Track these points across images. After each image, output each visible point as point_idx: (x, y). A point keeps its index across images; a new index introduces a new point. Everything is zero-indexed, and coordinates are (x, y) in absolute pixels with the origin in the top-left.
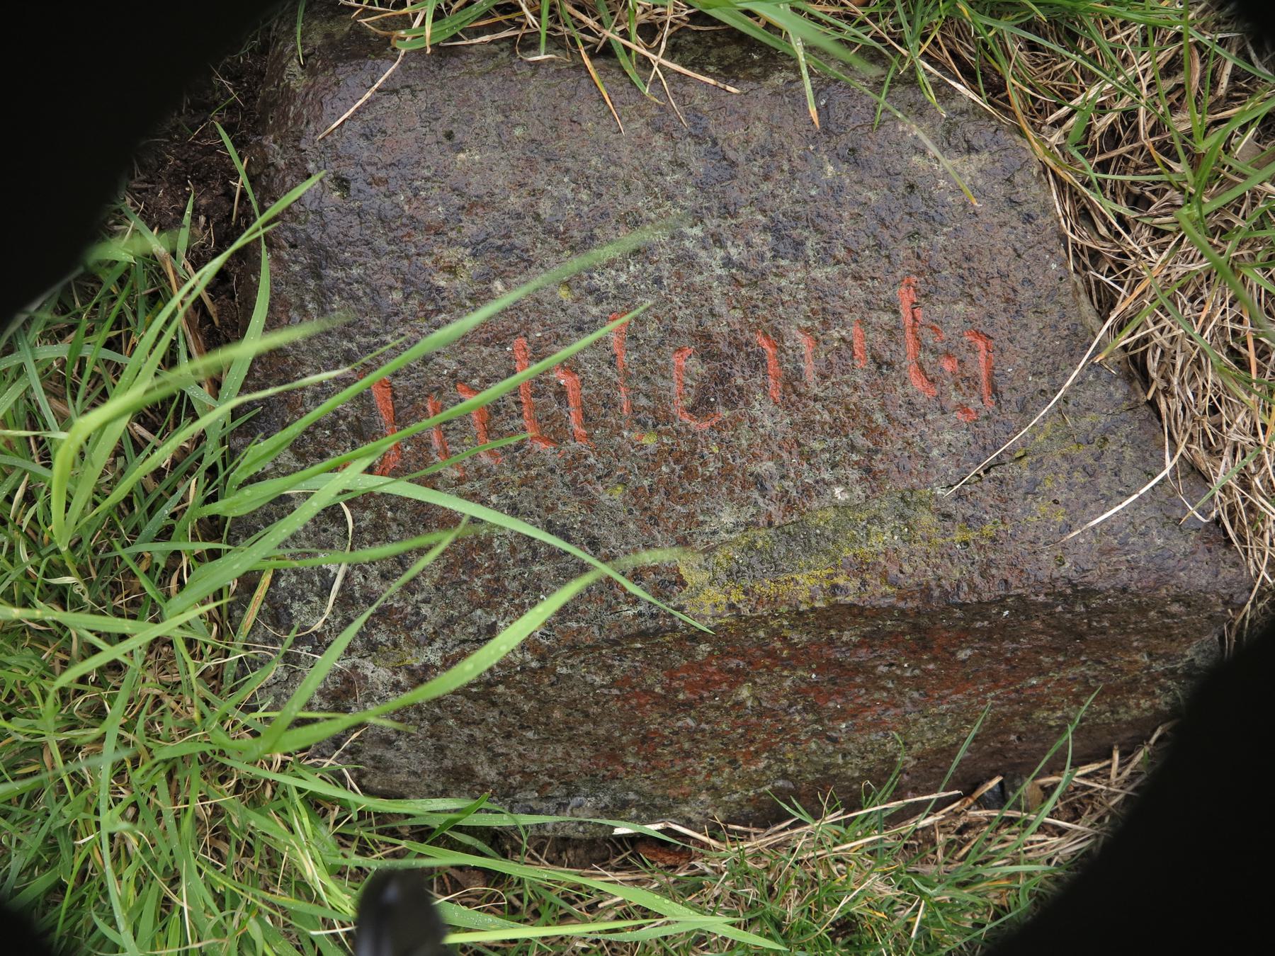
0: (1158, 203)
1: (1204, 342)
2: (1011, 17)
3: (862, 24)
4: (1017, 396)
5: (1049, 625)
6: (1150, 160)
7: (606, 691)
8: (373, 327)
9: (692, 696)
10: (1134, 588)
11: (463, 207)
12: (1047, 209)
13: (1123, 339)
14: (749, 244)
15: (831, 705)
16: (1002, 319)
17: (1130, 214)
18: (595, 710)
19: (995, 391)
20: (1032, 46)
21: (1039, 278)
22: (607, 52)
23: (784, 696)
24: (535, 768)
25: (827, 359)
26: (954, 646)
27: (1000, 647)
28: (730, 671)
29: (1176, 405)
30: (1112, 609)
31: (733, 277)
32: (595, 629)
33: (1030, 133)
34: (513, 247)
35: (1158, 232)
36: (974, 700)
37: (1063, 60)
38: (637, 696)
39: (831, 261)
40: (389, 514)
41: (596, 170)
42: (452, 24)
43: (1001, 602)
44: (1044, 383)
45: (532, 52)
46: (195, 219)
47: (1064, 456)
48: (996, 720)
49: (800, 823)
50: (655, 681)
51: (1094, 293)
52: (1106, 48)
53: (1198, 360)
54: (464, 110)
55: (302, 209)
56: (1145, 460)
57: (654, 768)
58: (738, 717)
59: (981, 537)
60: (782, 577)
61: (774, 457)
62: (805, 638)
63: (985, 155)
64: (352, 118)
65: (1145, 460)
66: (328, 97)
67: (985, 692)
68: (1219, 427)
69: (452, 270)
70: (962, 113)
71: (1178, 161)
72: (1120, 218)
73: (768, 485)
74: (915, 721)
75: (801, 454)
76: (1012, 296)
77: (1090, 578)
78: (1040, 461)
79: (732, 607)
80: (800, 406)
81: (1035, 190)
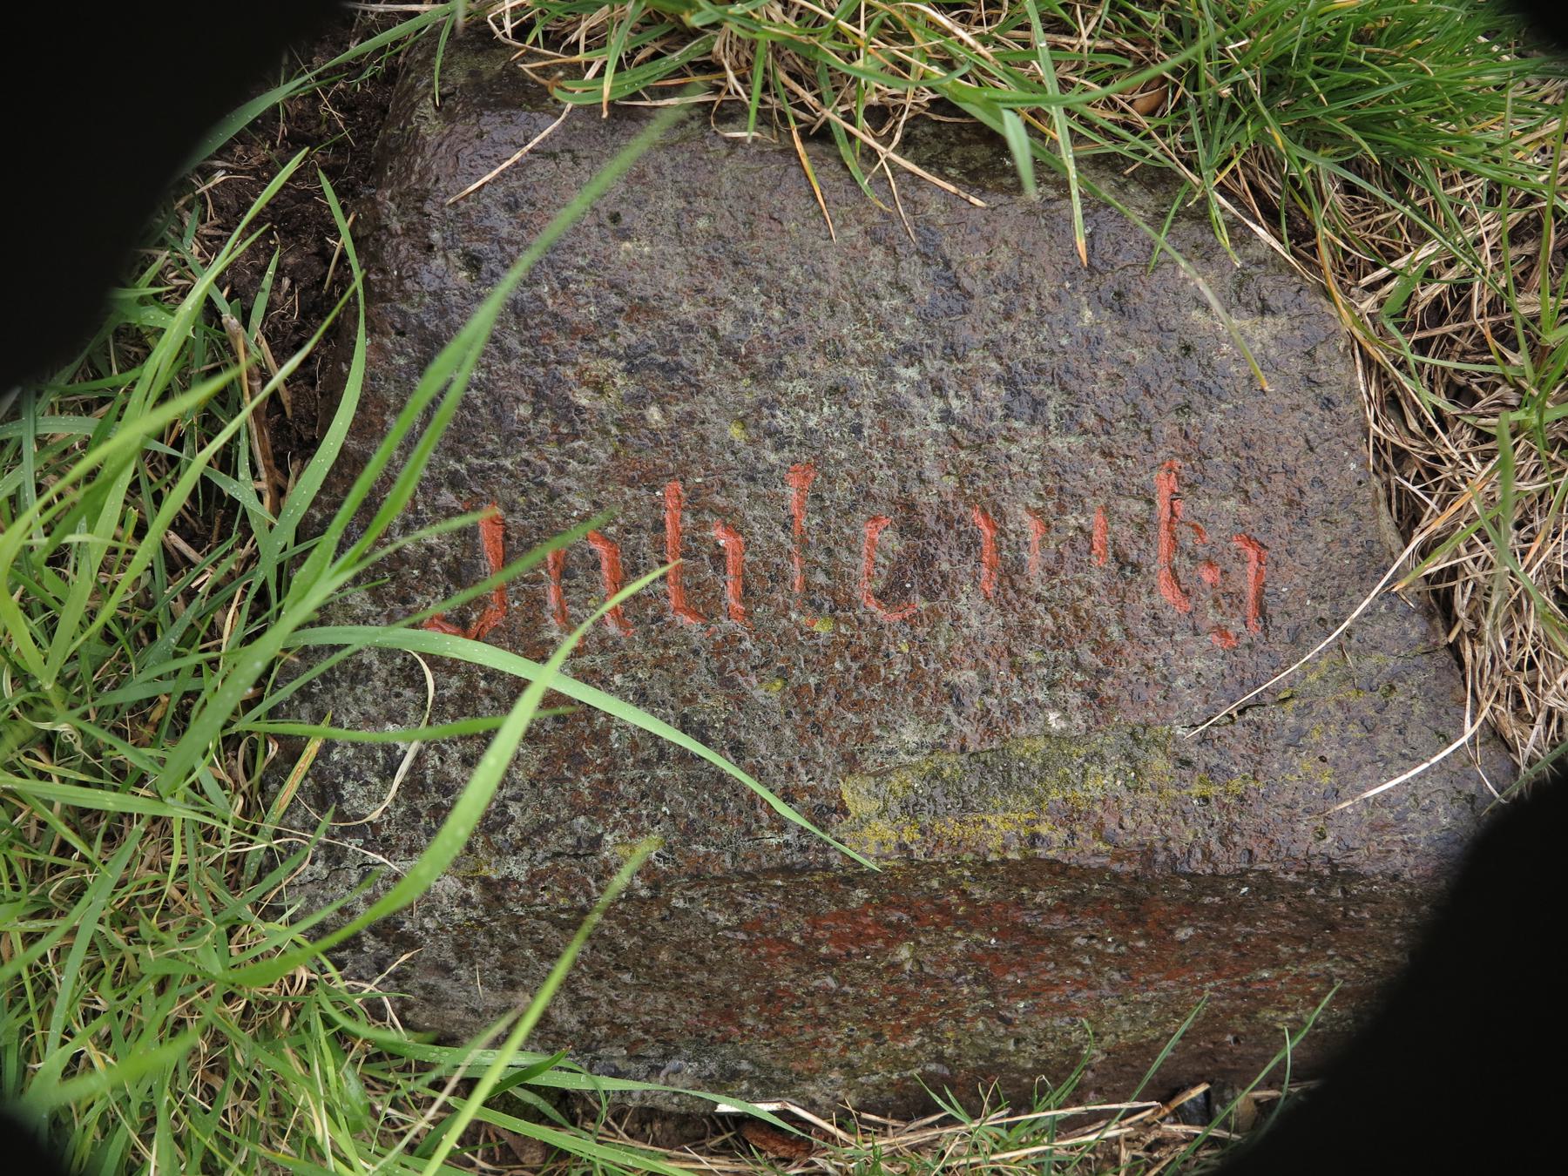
0: (1486, 399)
1: (1529, 579)
2: (1331, 151)
3: (1148, 137)
4: (1291, 623)
5: (1295, 910)
6: (1481, 343)
7: (730, 935)
8: (490, 447)
9: (838, 951)
10: (1407, 876)
11: (622, 310)
12: (1351, 393)
13: (1431, 567)
14: (976, 397)
15: (1010, 978)
16: (1282, 525)
17: (1450, 410)
18: (713, 956)
19: (1262, 610)
20: (1349, 188)
21: (1333, 481)
22: (822, 136)
23: (953, 963)
24: (627, 1019)
25: (1058, 551)
26: (1173, 922)
27: (1231, 930)
28: (890, 925)
29: (1484, 654)
30: (1375, 899)
31: (950, 433)
32: (727, 858)
33: (1338, 296)
34: (679, 366)
35: (1483, 436)
36: (1188, 990)
37: (1387, 210)
38: (768, 944)
39: (1077, 430)
40: (483, 684)
41: (795, 282)
42: (635, 79)
43: (1240, 877)
44: (1324, 610)
45: (730, 125)
46: (277, 281)
47: (1339, 703)
48: (1211, 1016)
49: (949, 1121)
50: (794, 928)
51: (1394, 500)
52: (1444, 202)
53: (1518, 603)
54: (637, 188)
55: (417, 287)
56: (1438, 717)
57: (777, 1034)
58: (891, 982)
59: (1226, 794)
60: (970, 817)
61: (977, 665)
62: (988, 894)
63: (1283, 320)
64: (495, 181)
65: (1438, 717)
66: (467, 152)
67: (1202, 981)
68: (1533, 686)
69: (598, 387)
70: (1259, 263)
71: (1516, 349)
72: (1436, 410)
73: (966, 700)
74: (1112, 1008)
75: (1012, 666)
76: (1297, 498)
77: (1356, 859)
78: (1309, 706)
79: (902, 847)
80: (1018, 605)
81: (1339, 369)
